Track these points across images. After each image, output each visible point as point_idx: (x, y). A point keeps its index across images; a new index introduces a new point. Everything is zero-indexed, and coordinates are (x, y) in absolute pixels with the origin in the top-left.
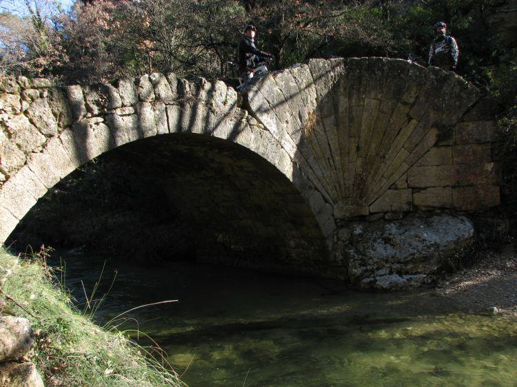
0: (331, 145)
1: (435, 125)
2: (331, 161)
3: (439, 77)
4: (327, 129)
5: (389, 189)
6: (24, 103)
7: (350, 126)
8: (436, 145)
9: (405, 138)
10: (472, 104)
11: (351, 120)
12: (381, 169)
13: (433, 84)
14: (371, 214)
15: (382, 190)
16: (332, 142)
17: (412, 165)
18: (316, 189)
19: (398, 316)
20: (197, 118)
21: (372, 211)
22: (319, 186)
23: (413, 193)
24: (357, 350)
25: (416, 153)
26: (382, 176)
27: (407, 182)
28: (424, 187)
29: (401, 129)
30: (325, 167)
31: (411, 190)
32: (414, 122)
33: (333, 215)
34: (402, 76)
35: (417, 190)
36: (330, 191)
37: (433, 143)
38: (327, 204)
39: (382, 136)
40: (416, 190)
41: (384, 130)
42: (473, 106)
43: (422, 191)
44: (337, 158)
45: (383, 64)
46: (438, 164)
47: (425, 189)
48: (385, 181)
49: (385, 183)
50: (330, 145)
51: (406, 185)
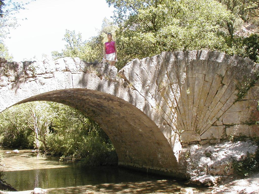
29: (218, 91)
31: (224, 126)
51: (222, 123)
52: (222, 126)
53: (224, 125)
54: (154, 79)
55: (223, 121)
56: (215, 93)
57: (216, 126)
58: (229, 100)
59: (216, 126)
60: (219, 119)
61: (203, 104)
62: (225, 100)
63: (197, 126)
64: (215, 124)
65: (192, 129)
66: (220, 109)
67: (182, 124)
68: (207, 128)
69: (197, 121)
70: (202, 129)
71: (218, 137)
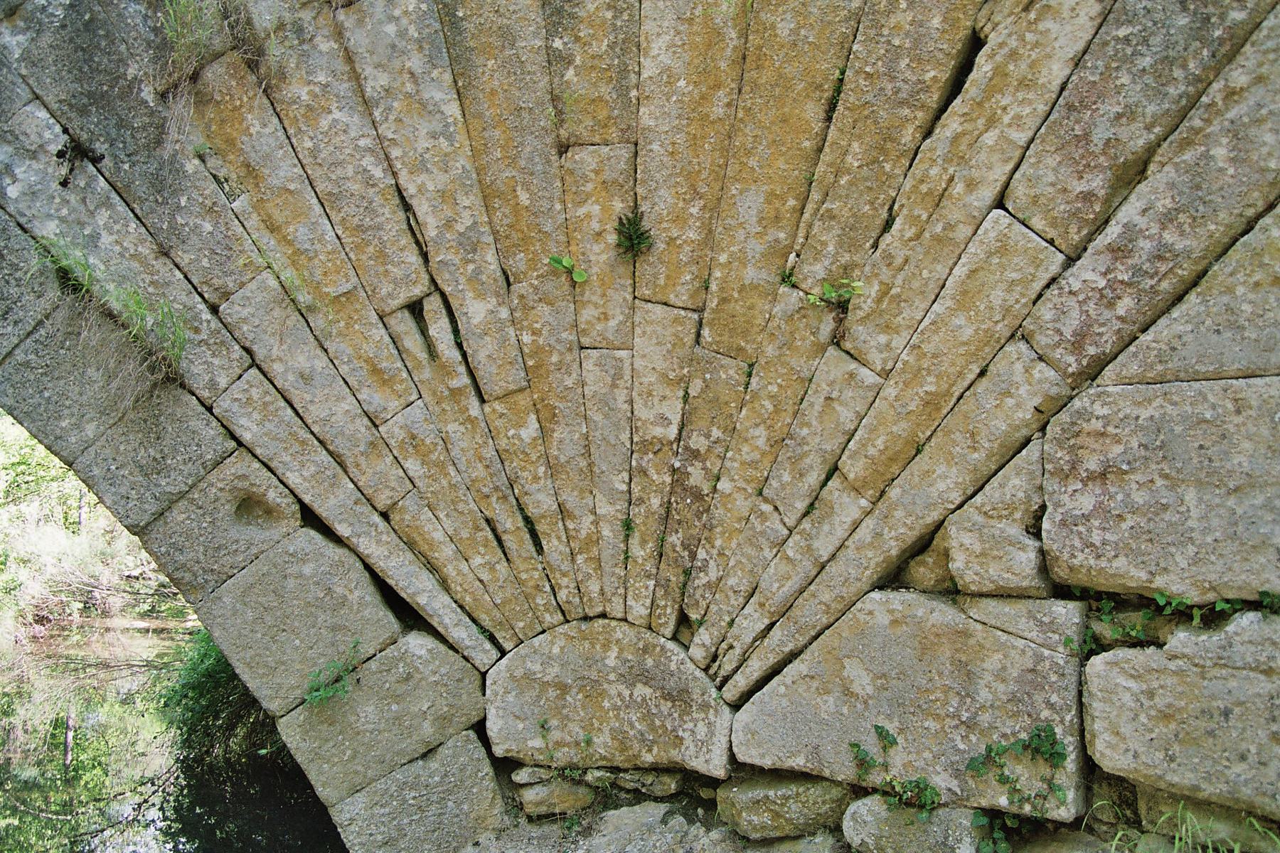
0: (422, 208)
2: (439, 328)
4: (376, 81)
5: (880, 585)
7: (557, 61)
12: (645, 218)
14: (741, 771)
16: (431, 182)
17: (1092, 372)
18: (310, 518)
20: (769, 785)
23: (1093, 646)
25: (1118, 252)
27: (1035, 531)
29: (976, 43)
31: (1067, 612)
33: (480, 728)
35: (1135, 621)
36: (445, 553)
38: (417, 643)
39: (813, 112)
41: (827, 67)
43: (1180, 638)
44: (475, 311)
48: (846, 506)
50: (407, 207)
51: (1026, 559)
52: (1022, 606)
53: (1062, 591)
54: (641, 219)
55: (1046, 525)
56: (937, 74)
57: (951, 591)
58: (1159, 178)
59: (951, 591)
60: (169, 257)
61: (342, 22)
62: (1097, 183)
63: (687, 573)
64: (924, 571)
65: (639, 610)
66: (1003, 330)
67: (518, 542)
68: (810, 612)
69: (684, 508)
70: (752, 621)
71: (954, 785)
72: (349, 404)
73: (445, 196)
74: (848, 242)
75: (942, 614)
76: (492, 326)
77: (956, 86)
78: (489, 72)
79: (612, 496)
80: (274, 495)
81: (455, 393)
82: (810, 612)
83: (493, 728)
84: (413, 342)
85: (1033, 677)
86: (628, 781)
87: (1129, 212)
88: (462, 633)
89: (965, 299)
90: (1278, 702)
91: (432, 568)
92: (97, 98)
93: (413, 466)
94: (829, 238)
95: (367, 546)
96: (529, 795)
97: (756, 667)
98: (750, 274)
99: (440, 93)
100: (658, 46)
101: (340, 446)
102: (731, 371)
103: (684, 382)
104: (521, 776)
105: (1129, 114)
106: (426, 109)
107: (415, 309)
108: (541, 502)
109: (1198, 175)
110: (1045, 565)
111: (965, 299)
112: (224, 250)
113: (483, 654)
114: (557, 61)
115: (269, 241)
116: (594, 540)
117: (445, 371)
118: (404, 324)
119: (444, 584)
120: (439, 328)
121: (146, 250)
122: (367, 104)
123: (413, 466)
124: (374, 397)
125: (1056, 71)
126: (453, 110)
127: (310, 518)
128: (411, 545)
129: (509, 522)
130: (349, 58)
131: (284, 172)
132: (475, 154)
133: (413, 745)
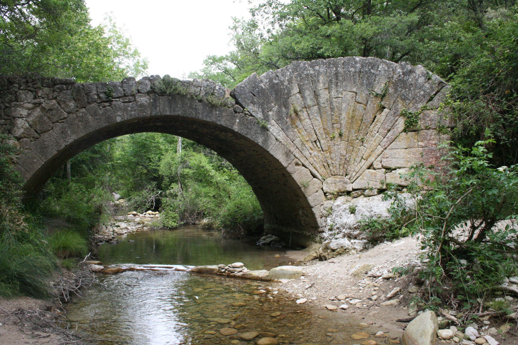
0: (316, 131)
1: (403, 115)
2: (318, 144)
3: (405, 70)
6: (55, 93)
8: (405, 131)
9: (379, 125)
10: (434, 93)
11: (332, 109)
13: (400, 76)
15: (361, 170)
17: (386, 148)
18: (303, 165)
19: (32, 291)
21: (355, 188)
22: (306, 163)
24: (184, 319)
25: (388, 138)
26: (362, 158)
28: (394, 168)
29: (375, 117)
30: (313, 147)
32: (386, 110)
33: (322, 189)
34: (372, 71)
36: (318, 169)
37: (402, 128)
38: (315, 179)
40: (389, 169)
42: (435, 95)
44: (322, 142)
45: (356, 63)
46: (405, 147)
47: (395, 169)
49: (365, 164)
57: (374, 169)
62: (386, 131)
64: (372, 168)
67: (327, 167)
68: (360, 172)
72: (308, 152)
73: (319, 129)
74: (363, 136)
75: (374, 171)
76: (324, 143)
77: (373, 121)
78: (324, 116)
79: (338, 161)
80: (300, 163)
81: (320, 151)
82: (360, 172)
83: (324, 189)
84: (315, 145)
85: (381, 176)
86: (340, 194)
87: (389, 134)
88: (320, 178)
89: (375, 141)
90: (517, 117)
91: (317, 170)
92: (280, 119)
93: (315, 159)
94: (361, 135)
95: (310, 168)
96: (328, 196)
97: (355, 179)
98: (353, 138)
99: (319, 118)
100: (343, 115)
101: (307, 157)
102: (351, 148)
103: (346, 149)
104: (327, 194)
105: (388, 126)
106: (317, 120)
107: (315, 142)
108: (330, 162)
109: (394, 132)
110: (382, 166)
111: (375, 141)
112: (294, 135)
113: (323, 181)
114: (332, 115)
115: (299, 134)
116: (336, 166)
117: (319, 148)
118: (314, 143)
119: (318, 172)
120: (318, 144)
121: (285, 136)
122: (310, 119)
123: (315, 159)
124: (311, 151)
125: (382, 121)
126: (320, 120)
127: (303, 165)
128: (315, 168)
129: (326, 165)
130: (308, 114)
131: (301, 126)
132: (323, 124)
133: (315, 191)
